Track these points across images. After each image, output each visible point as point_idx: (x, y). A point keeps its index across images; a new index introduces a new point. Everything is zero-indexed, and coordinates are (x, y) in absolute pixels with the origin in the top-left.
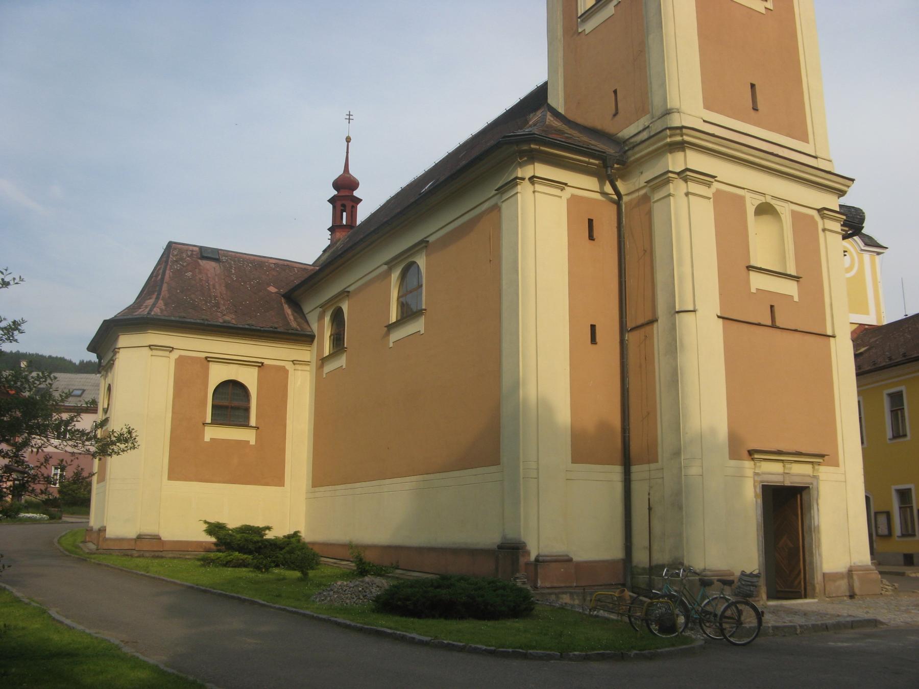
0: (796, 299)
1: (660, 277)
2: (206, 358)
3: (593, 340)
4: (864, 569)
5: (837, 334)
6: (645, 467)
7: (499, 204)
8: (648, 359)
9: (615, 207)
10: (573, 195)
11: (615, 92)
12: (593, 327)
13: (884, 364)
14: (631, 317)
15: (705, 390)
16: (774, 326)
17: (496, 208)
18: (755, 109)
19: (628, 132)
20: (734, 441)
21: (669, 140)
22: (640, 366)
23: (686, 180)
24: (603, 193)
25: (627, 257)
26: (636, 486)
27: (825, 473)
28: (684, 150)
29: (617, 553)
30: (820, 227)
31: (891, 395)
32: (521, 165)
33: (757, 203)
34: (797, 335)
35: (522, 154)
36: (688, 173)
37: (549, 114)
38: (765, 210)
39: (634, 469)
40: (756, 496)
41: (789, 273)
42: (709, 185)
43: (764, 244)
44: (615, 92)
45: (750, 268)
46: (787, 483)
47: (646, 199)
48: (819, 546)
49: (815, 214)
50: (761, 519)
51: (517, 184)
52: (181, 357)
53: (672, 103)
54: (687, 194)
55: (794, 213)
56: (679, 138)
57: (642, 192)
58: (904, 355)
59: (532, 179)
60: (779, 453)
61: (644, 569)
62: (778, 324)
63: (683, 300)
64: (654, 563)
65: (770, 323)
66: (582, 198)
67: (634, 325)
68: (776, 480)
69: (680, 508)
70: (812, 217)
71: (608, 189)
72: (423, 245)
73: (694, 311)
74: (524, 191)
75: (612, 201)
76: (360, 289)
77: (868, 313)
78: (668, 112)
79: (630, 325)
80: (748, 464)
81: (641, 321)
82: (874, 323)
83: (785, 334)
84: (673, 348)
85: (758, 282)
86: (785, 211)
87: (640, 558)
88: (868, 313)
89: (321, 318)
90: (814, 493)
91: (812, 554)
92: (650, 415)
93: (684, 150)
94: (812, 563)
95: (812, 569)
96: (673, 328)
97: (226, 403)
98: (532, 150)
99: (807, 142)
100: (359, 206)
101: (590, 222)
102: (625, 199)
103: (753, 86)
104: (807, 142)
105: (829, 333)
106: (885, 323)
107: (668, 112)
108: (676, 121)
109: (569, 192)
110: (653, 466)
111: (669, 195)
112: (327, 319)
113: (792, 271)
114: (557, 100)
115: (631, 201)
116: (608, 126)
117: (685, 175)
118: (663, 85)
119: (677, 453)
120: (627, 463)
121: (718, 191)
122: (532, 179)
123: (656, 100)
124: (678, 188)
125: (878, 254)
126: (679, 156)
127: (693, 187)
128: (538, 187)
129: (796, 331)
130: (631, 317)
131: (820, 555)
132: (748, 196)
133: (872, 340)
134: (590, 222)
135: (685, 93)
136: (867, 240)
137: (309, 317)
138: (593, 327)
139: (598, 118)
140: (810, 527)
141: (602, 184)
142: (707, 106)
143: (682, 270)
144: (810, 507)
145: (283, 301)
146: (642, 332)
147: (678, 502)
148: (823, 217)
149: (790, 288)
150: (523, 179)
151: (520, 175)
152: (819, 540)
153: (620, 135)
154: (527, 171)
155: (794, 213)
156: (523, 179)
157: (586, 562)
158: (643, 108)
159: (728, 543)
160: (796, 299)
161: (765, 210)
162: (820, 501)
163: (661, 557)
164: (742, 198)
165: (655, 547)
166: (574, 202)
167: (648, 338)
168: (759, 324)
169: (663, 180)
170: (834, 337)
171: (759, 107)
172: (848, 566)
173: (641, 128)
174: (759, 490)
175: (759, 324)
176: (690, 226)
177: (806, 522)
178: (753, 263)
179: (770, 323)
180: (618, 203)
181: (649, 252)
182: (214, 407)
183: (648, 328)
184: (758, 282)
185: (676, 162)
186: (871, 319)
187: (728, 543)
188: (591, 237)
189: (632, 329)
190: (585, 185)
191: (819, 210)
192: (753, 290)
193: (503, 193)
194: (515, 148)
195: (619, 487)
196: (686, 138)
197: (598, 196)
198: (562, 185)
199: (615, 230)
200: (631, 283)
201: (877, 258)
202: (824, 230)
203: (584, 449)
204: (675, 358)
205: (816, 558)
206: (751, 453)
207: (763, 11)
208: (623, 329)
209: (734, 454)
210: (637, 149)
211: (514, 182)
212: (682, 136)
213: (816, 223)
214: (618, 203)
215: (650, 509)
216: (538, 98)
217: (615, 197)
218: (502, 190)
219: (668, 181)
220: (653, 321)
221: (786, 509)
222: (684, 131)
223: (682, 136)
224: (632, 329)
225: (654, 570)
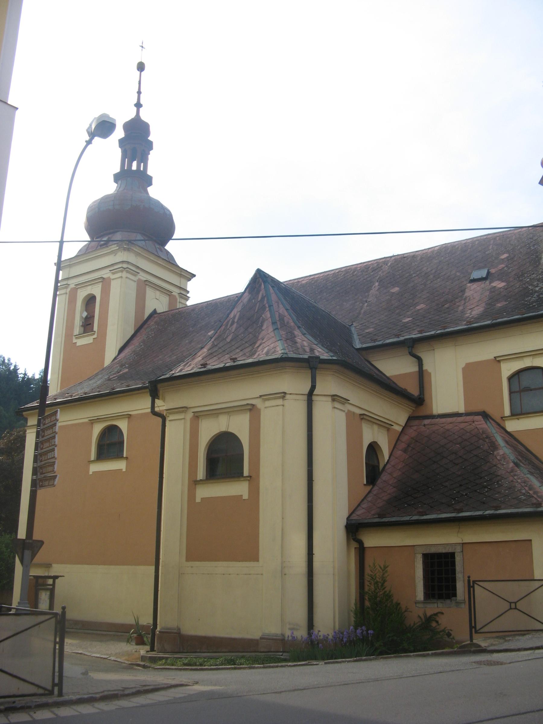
39: (535, 578)
68: (252, 564)
193: (265, 400)
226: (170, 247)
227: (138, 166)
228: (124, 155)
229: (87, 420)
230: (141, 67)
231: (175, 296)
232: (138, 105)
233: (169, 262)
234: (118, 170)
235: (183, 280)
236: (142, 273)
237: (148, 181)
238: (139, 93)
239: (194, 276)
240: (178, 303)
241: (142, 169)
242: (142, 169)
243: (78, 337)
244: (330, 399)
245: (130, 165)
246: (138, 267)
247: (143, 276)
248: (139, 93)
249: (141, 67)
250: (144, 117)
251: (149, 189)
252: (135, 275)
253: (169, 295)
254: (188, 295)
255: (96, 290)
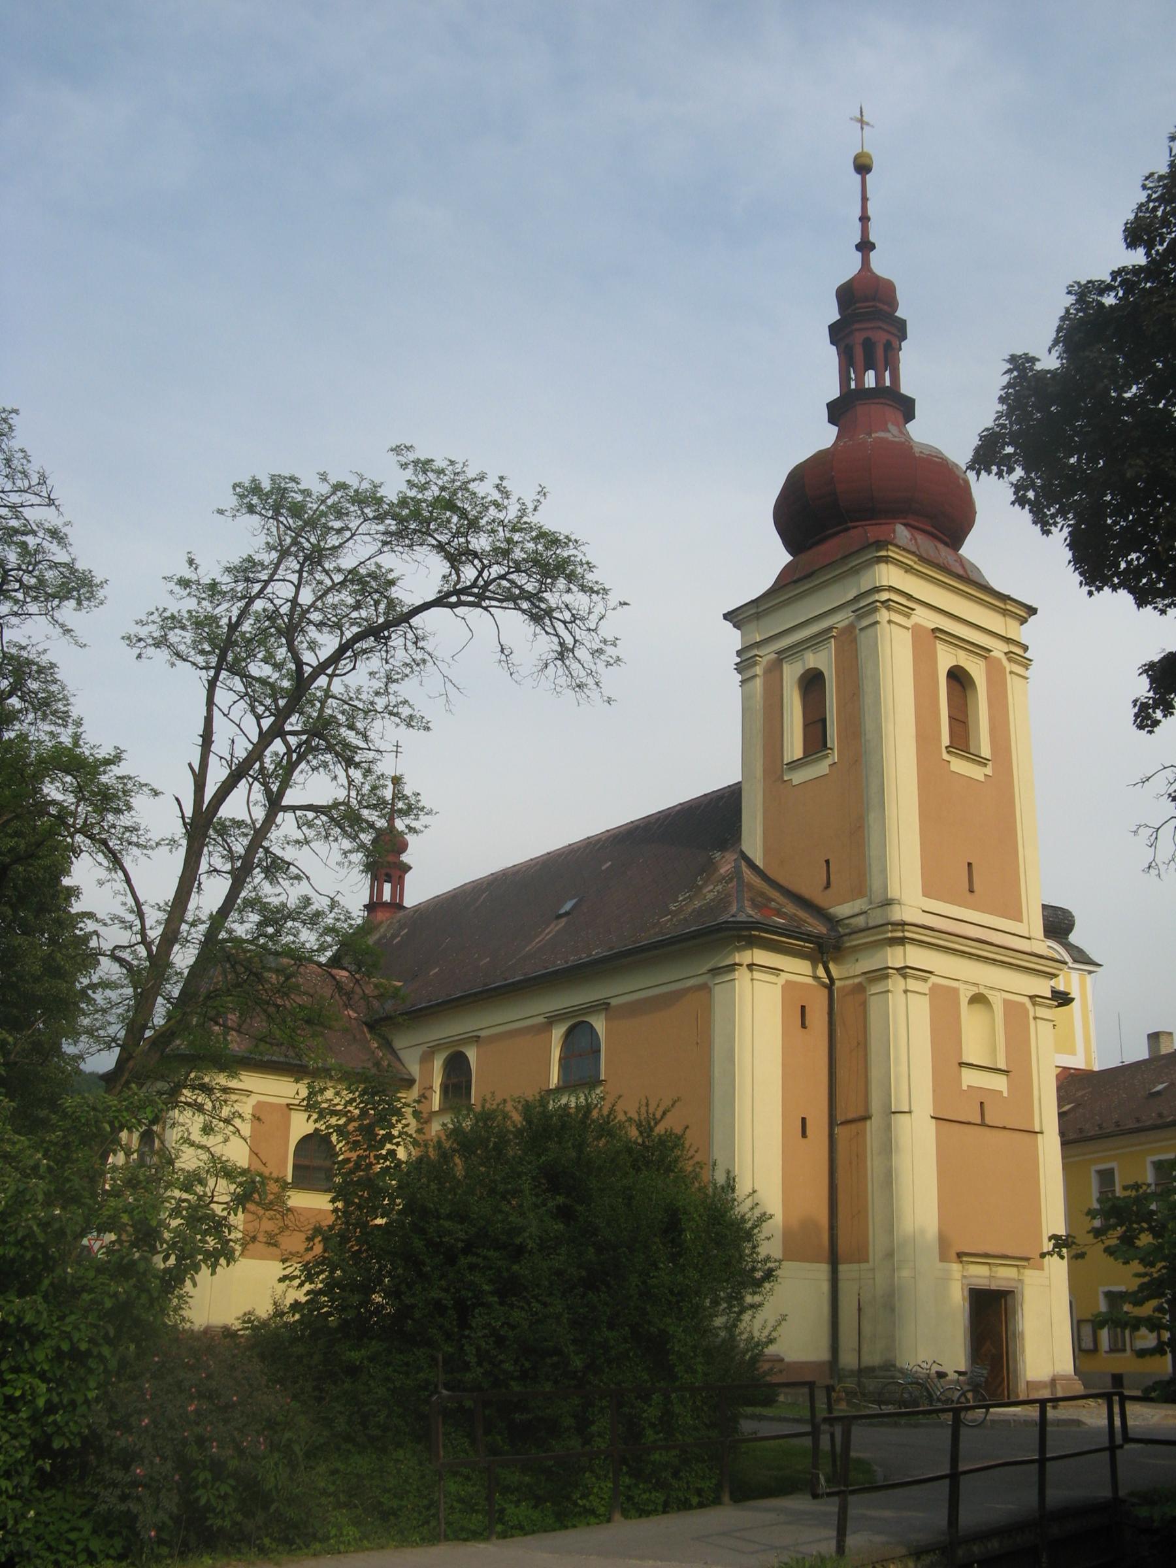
0: (1005, 1094)
1: (875, 1073)
2: (288, 1105)
3: (804, 1134)
4: (1065, 1378)
5: (1044, 1130)
6: (855, 1266)
7: (710, 984)
8: (860, 1158)
9: (826, 991)
10: (787, 981)
11: (827, 862)
12: (804, 1120)
13: (1092, 1133)
14: (844, 1113)
15: (917, 1190)
16: (983, 1124)
17: (705, 988)
18: (971, 891)
19: (842, 910)
20: (943, 1242)
21: (890, 935)
22: (851, 1163)
23: (905, 976)
24: (816, 978)
25: (838, 1046)
26: (843, 1286)
27: (1030, 1277)
28: (904, 945)
29: (820, 1353)
30: (1031, 1014)
31: (1099, 1172)
32: (740, 949)
33: (970, 994)
34: (1006, 1132)
35: (740, 938)
36: (908, 970)
37: (743, 863)
38: (978, 999)
39: (842, 1268)
40: (963, 1299)
41: (999, 1067)
42: (925, 980)
43: (978, 1037)
44: (827, 862)
45: (961, 1064)
46: (993, 1287)
47: (860, 989)
48: (1023, 1351)
49: (1026, 1000)
50: (967, 1323)
51: (734, 970)
52: (259, 1103)
53: (893, 893)
54: (906, 991)
55: (1006, 1001)
56: (900, 934)
57: (857, 980)
58: (1117, 1124)
59: (751, 966)
60: (986, 1256)
61: (852, 1371)
62: (988, 1121)
63: (899, 1101)
64: (863, 1365)
65: (979, 1121)
66: (795, 983)
67: (843, 1119)
68: (983, 1284)
69: (893, 1310)
70: (1023, 1004)
71: (821, 972)
72: (603, 1007)
73: (910, 1112)
74: (742, 977)
75: (824, 985)
76: (493, 1039)
77: (1073, 1052)
78: (888, 903)
79: (839, 1119)
80: (955, 1267)
81: (851, 1116)
82: (1082, 1066)
83: (995, 1132)
84: (888, 1148)
85: (970, 1078)
86: (996, 999)
87: (848, 1360)
88: (1073, 1052)
89: (427, 1058)
90: (1018, 1297)
91: (1015, 1361)
92: (861, 1213)
93: (904, 945)
94: (1016, 1370)
95: (1016, 1377)
96: (888, 1127)
97: (306, 1162)
98: (751, 936)
99: (1021, 922)
100: (407, 876)
101: (803, 1007)
102: (838, 984)
103: (969, 864)
104: (1021, 922)
105: (1037, 1130)
106: (1096, 1069)
107: (888, 903)
108: (897, 914)
109: (784, 977)
110: (864, 1266)
111: (888, 991)
112: (438, 1064)
113: (1003, 1067)
114: (753, 842)
115: (844, 987)
116: (820, 899)
117: (903, 971)
118: (884, 871)
119: (890, 1255)
120: (834, 1261)
121: (934, 984)
122: (751, 966)
123: (876, 885)
124: (896, 984)
125: (1090, 972)
126: (899, 950)
127: (912, 984)
128: (757, 975)
129: (1004, 1128)
130: (844, 1113)
131: (1024, 1362)
132: (962, 987)
133: (1080, 1094)
134: (803, 1007)
135: (908, 890)
136: (1076, 954)
137: (403, 1055)
138: (804, 1120)
139: (809, 885)
140: (1014, 1334)
141: (815, 967)
142: (926, 894)
143: (898, 1069)
144: (1014, 1313)
145: (365, 1030)
146: (853, 1127)
147: (891, 1303)
148: (1034, 1004)
149: (999, 1083)
150: (741, 965)
151: (737, 961)
152: (1023, 1346)
153: (832, 910)
154: (746, 957)
155: (1006, 1001)
156: (741, 965)
157: (795, 1363)
158: (860, 888)
159: (937, 1345)
160: (1005, 1094)
161: (978, 999)
162: (1025, 1307)
163: (872, 1358)
164: (956, 991)
165: (865, 1349)
166: (788, 987)
167: (861, 1135)
168: (969, 1123)
169: (881, 974)
170: (1042, 1133)
171: (976, 888)
172: (1051, 1374)
173: (857, 911)
174: (966, 1293)
175: (969, 1123)
176: (906, 1024)
177: (1011, 1327)
178: (966, 1059)
179: (979, 1121)
180: (830, 987)
181: (863, 1045)
182: (294, 1166)
183: (860, 1124)
184: (970, 1078)
185: (895, 957)
186: (1077, 1062)
187: (937, 1345)
188: (804, 1026)
189: (842, 1123)
190: (798, 969)
191: (1031, 997)
192: (964, 1088)
193: (714, 975)
194: (735, 933)
195: (825, 1287)
196: (907, 934)
197: (810, 981)
198: (776, 971)
199: (826, 1016)
200: (842, 1074)
201: (1089, 978)
202: (1035, 1018)
203: (796, 1248)
204: (890, 1159)
205: (1020, 1365)
206: (960, 1255)
207: (982, 778)
208: (832, 1123)
209: (943, 1258)
210: (853, 936)
211: (732, 967)
212: (903, 931)
213: (1027, 1011)
214: (830, 987)
215: (859, 1309)
216: (710, 821)
217: (827, 981)
218: (716, 971)
219: (887, 976)
220: (866, 1118)
221: (991, 1313)
222: (906, 927)
223: (903, 931)
224: (842, 1123)
225: (863, 1372)
226: (971, 549)
227: (879, 378)
228: (847, 361)
229: (541, 1019)
230: (863, 167)
231: (999, 660)
232: (865, 246)
233: (970, 581)
234: (835, 393)
235: (1013, 624)
236: (920, 611)
237: (907, 408)
238: (864, 219)
239: (1032, 611)
240: (1008, 676)
241: (888, 384)
242: (888, 384)
243: (795, 765)
244: (1073, 938)
245: (860, 380)
246: (910, 597)
247: (926, 619)
248: (864, 219)
249: (863, 167)
250: (881, 265)
251: (910, 426)
252: (908, 616)
253: (986, 658)
254: (405, 858)
255: (822, 660)
